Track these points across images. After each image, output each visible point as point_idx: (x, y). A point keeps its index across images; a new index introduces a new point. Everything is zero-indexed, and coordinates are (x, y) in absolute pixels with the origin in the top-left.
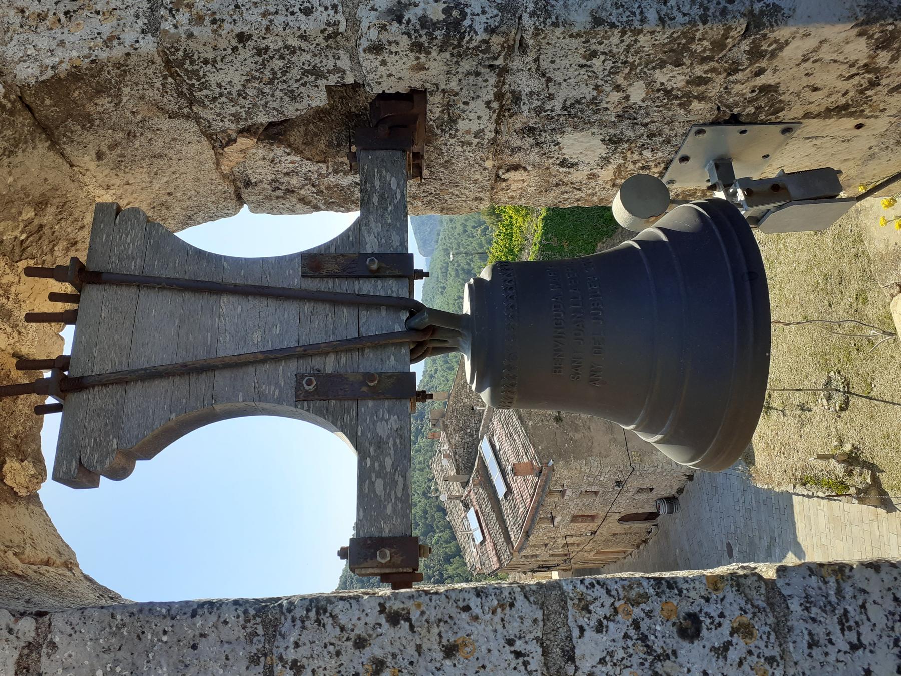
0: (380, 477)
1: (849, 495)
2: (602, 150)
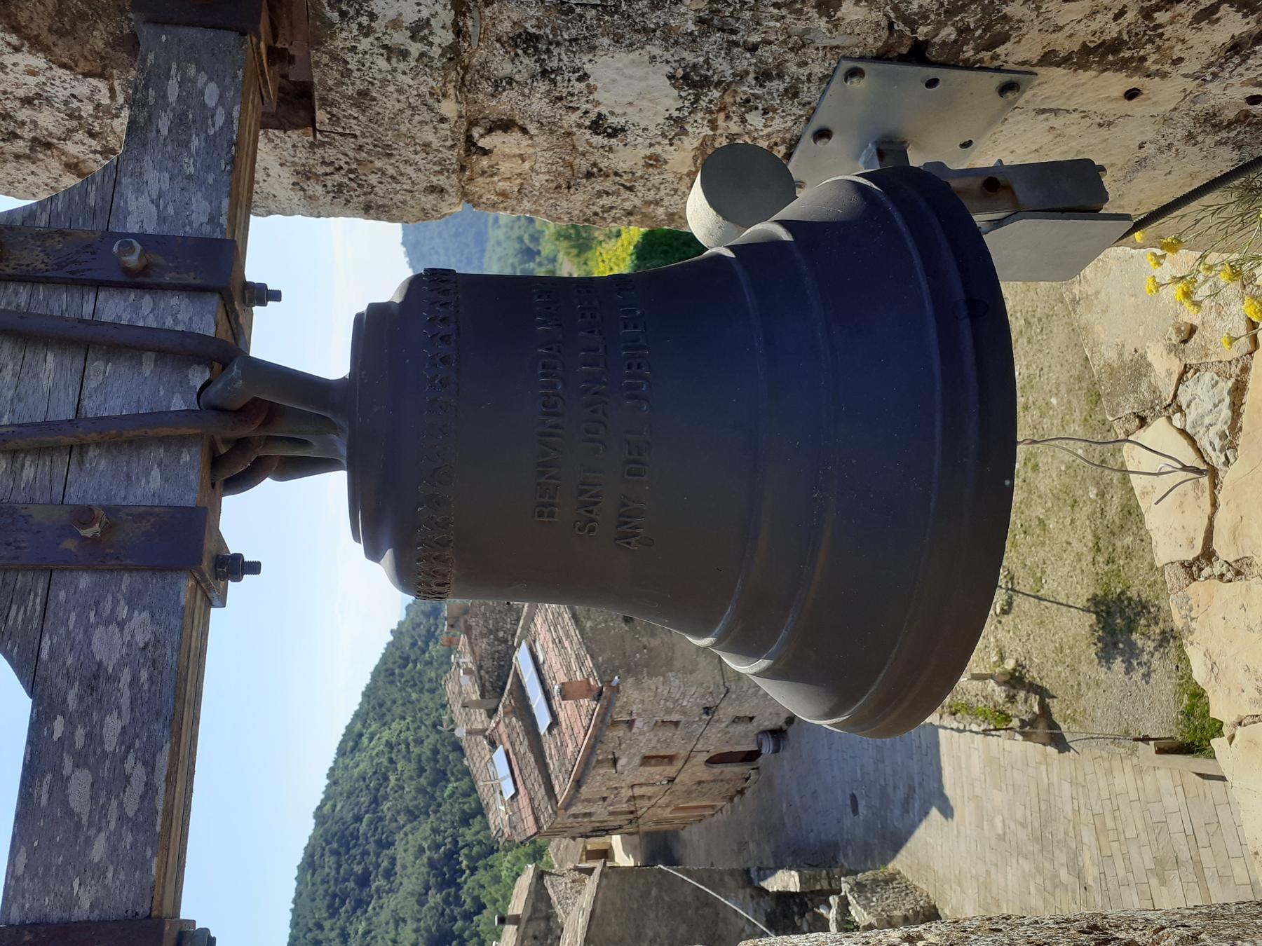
0: (86, 764)
1: (1010, 729)
2: (669, 100)
